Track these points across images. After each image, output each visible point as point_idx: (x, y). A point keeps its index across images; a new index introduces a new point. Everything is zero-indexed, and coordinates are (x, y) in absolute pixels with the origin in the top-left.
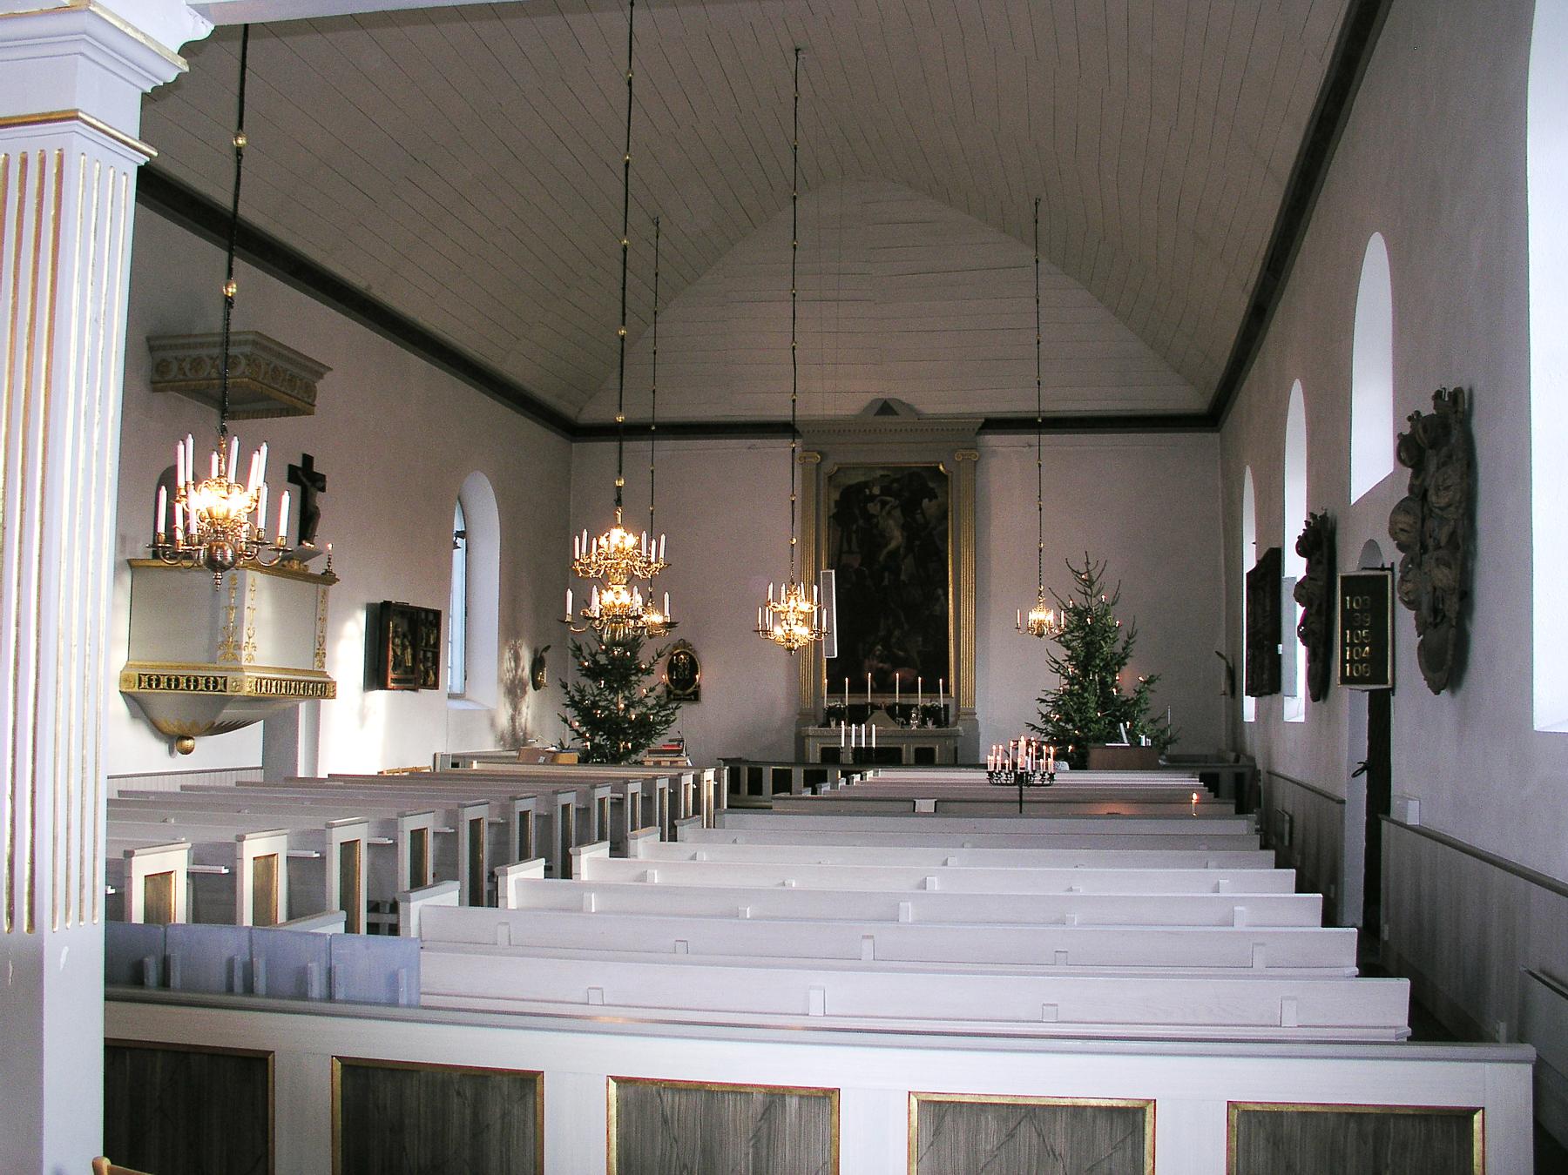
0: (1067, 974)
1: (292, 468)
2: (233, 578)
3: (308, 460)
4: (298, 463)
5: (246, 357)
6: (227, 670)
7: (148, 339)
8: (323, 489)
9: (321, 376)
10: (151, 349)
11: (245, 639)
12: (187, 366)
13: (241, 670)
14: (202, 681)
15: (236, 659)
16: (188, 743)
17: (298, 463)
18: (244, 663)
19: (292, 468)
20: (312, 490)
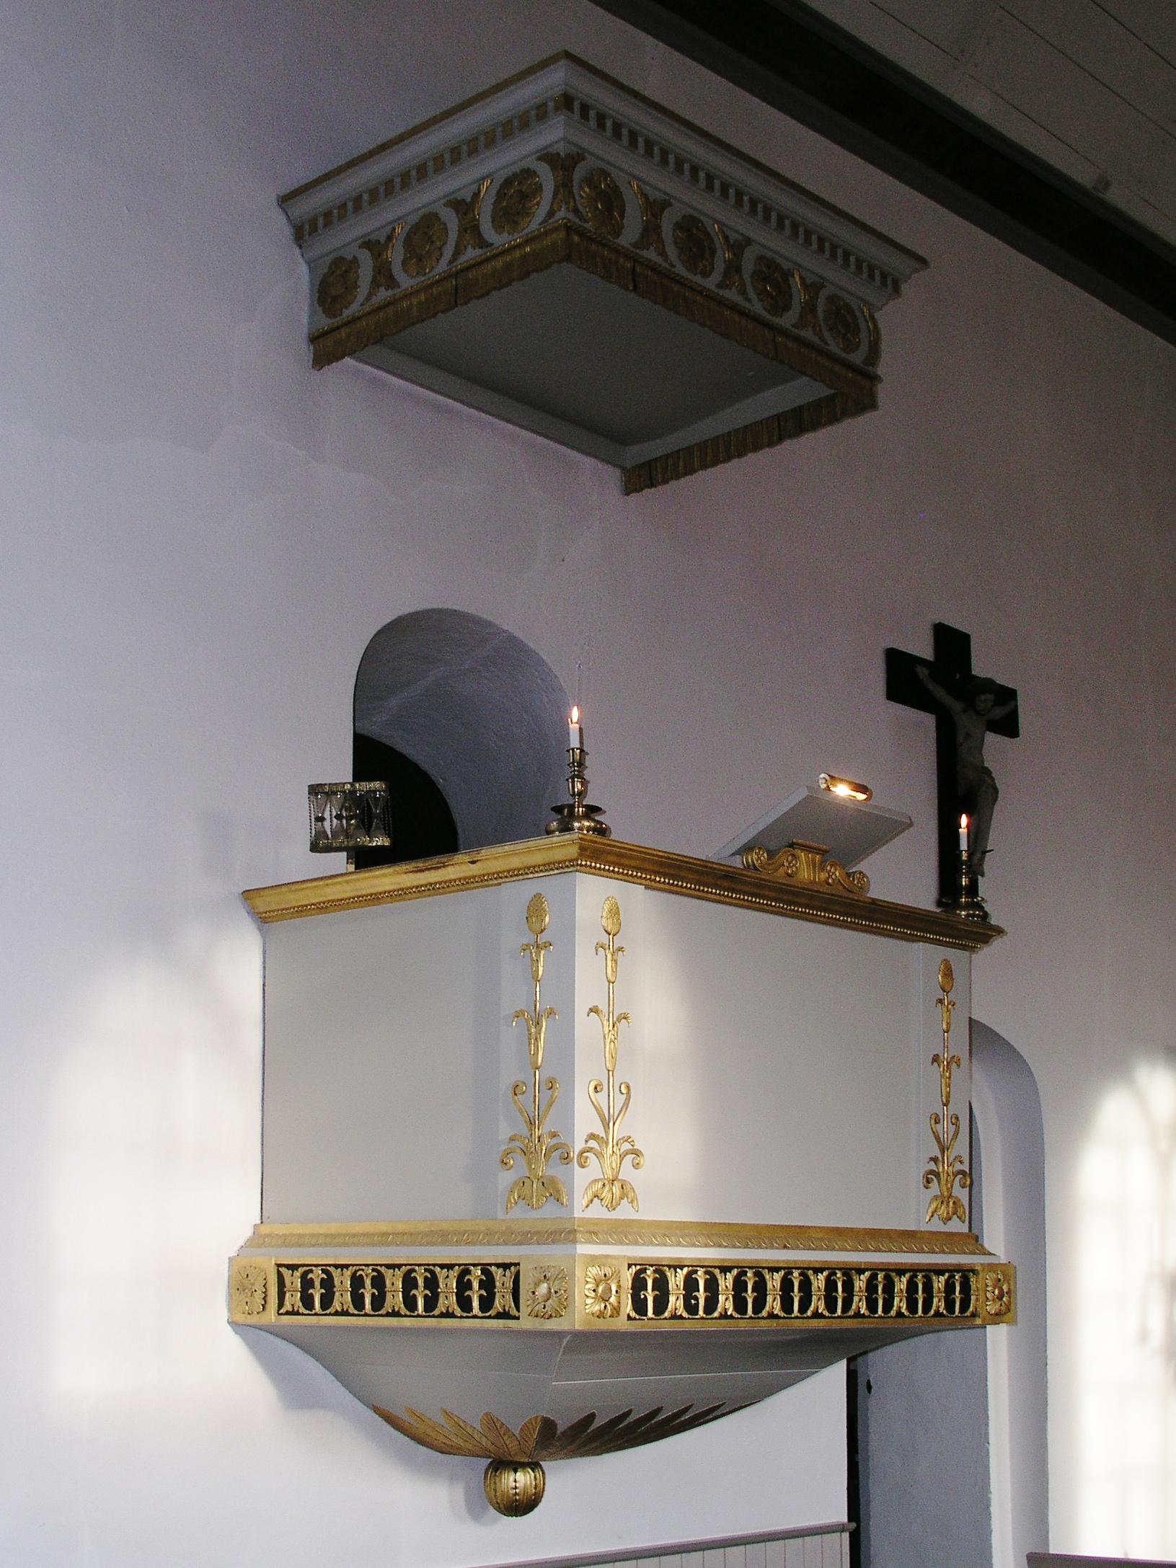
0: (419, 891)
1: (897, 663)
2: (535, 908)
3: (952, 643)
4: (923, 648)
5: (549, 158)
6: (526, 1238)
7: (285, 201)
8: (1009, 727)
9: (893, 285)
10: (302, 233)
11: (584, 1122)
12: (396, 255)
13: (565, 1234)
14: (448, 1283)
15: (554, 1191)
16: (521, 1480)
17: (923, 648)
18: (582, 1208)
19: (897, 663)
20: (966, 722)
